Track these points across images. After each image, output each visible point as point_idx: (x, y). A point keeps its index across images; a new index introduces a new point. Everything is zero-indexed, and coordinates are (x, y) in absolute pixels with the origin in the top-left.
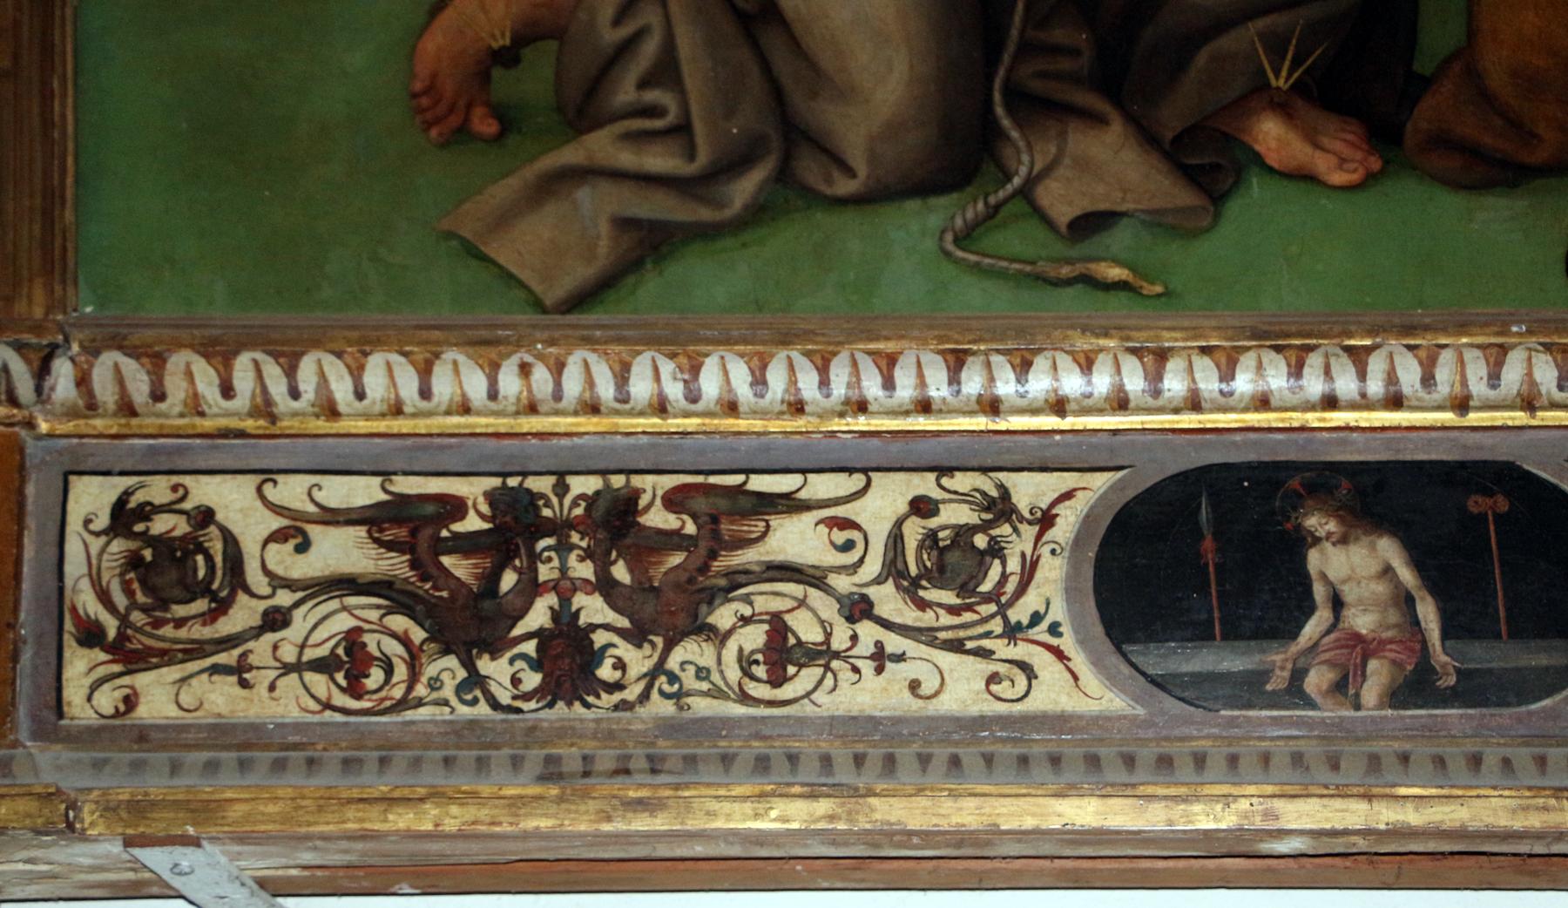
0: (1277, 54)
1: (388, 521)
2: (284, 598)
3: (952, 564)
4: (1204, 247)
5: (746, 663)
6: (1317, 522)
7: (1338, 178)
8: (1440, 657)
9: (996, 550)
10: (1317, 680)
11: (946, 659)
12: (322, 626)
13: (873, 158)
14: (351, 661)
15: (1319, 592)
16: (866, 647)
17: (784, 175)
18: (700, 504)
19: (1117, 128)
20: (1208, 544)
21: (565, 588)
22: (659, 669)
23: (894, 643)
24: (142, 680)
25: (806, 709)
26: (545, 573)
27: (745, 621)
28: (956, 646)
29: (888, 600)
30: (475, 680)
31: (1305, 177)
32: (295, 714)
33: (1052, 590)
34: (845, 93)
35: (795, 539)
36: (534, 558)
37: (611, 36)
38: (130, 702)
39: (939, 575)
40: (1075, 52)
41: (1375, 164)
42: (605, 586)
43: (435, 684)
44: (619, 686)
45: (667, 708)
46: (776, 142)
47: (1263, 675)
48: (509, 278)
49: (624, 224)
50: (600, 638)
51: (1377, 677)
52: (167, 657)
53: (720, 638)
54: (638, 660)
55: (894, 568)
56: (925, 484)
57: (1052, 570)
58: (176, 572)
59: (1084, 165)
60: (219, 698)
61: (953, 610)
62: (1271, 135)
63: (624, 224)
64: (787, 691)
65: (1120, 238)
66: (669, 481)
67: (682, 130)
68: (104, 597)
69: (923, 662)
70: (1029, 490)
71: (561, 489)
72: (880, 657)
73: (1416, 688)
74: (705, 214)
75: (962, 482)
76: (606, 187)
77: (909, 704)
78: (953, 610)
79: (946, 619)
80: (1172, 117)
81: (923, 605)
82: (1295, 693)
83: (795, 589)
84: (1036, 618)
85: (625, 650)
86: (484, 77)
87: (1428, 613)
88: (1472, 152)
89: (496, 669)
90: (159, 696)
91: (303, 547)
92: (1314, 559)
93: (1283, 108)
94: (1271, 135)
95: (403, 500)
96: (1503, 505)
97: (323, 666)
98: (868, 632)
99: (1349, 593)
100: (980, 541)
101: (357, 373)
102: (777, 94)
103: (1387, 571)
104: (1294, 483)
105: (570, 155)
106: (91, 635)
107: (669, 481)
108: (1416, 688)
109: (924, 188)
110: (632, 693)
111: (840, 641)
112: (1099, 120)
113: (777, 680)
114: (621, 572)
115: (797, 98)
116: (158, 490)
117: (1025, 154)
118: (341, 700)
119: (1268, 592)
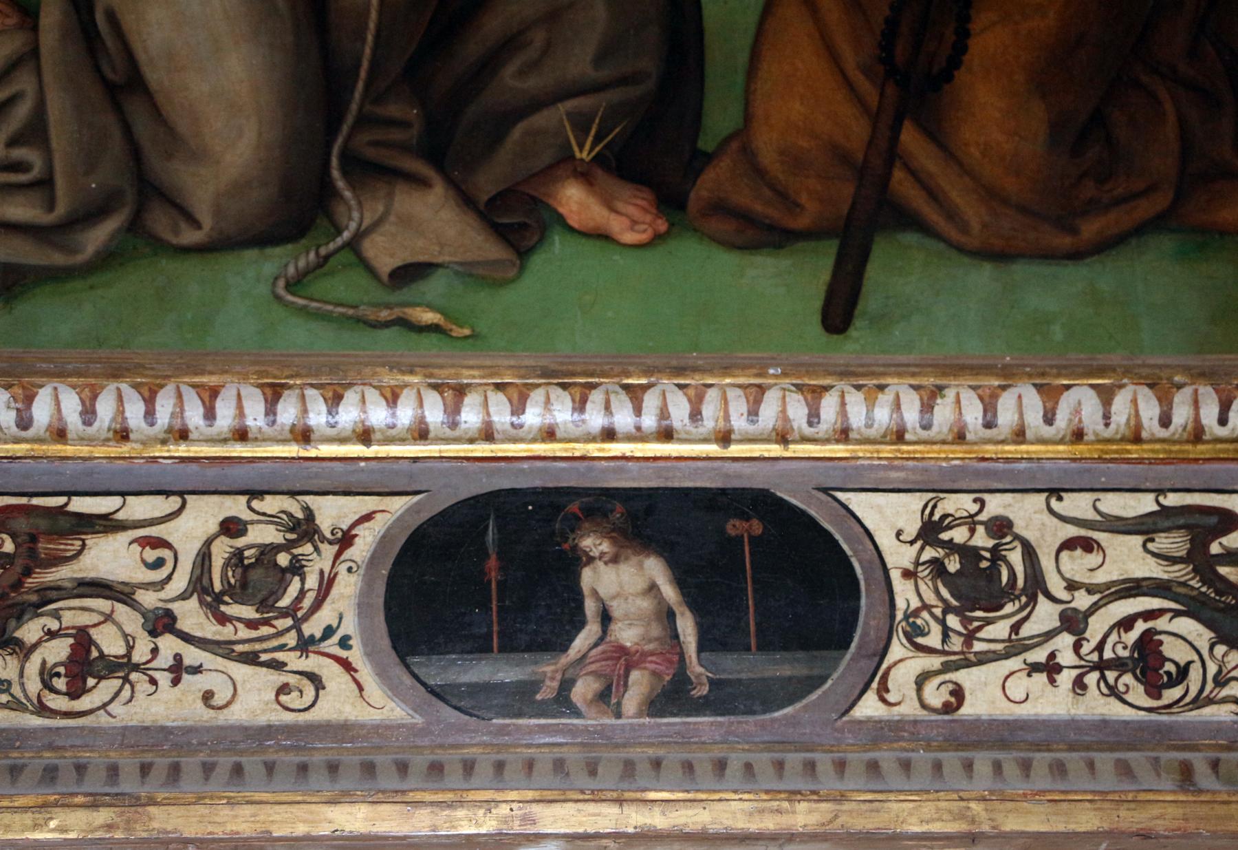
3: (254, 581)
4: (509, 295)
5: (47, 676)
6: (594, 543)
7: (629, 237)
8: (695, 668)
9: (297, 568)
11: (241, 671)
13: (218, 212)
15: (590, 607)
16: (165, 660)
17: (135, 226)
18: (22, 524)
23: (192, 655)
25: (102, 719)
27: (52, 635)
28: (251, 659)
29: (191, 616)
31: (602, 236)
33: (347, 605)
34: (199, 155)
35: (109, 557)
39: (240, 592)
40: (404, 124)
41: (662, 226)
46: (130, 196)
47: (533, 686)
51: (639, 685)
53: (25, 651)
55: (199, 586)
56: (236, 507)
57: (347, 587)
59: (406, 222)
61: (251, 624)
62: (573, 200)
64: (85, 703)
65: (435, 286)
67: (45, 184)
69: (218, 674)
70: (332, 512)
73: (672, 697)
74: (58, 259)
75: (271, 504)
78: (251, 624)
79: (244, 633)
80: (487, 183)
81: (223, 619)
82: (563, 702)
83: (103, 604)
84: (329, 632)
87: (687, 626)
88: (745, 218)
93: (585, 176)
94: (573, 200)
96: (757, 527)
98: (169, 645)
100: (283, 559)
102: (135, 153)
103: (653, 588)
104: (574, 507)
108: (672, 697)
109: (263, 239)
111: (141, 654)
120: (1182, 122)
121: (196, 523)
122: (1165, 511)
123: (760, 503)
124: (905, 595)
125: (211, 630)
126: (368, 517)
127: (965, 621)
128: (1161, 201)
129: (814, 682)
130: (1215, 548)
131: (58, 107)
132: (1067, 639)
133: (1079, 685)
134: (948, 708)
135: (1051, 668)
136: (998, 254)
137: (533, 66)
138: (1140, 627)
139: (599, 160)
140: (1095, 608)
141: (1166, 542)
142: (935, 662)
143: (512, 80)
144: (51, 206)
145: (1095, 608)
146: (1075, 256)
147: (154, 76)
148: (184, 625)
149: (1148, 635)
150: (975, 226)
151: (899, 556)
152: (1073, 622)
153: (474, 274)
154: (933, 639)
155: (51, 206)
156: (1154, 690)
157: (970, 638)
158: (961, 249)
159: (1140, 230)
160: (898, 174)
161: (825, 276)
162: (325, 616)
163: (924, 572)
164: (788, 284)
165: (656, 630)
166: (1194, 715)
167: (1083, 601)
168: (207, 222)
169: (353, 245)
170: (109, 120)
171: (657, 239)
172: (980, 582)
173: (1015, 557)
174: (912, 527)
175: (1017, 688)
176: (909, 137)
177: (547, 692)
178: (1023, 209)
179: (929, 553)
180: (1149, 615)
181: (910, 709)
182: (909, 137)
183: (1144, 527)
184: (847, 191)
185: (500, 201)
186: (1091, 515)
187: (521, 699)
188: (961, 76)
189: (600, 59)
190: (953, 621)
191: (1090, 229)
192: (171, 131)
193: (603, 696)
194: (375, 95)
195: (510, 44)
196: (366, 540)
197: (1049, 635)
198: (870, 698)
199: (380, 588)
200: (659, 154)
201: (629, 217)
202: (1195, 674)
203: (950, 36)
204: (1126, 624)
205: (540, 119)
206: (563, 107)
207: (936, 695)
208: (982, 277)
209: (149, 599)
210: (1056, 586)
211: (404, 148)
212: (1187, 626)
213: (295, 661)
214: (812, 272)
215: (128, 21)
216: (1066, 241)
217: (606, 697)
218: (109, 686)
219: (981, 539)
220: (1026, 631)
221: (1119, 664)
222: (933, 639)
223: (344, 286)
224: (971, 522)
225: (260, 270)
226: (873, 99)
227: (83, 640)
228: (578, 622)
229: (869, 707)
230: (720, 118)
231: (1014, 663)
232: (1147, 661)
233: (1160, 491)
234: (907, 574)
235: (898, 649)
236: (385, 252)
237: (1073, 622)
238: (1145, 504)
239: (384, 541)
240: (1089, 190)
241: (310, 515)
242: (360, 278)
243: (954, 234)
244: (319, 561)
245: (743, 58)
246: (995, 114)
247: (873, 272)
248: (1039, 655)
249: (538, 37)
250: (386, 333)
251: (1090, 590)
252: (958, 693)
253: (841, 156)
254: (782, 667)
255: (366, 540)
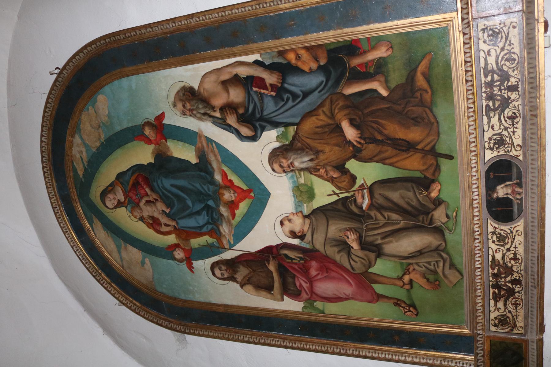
0: (422, 194)
1: (496, 298)
2: (507, 311)
3: (502, 239)
4: (450, 203)
5: (516, 263)
6: (495, 196)
7: (439, 187)
8: (515, 182)
9: (500, 234)
10: (518, 197)
11: (515, 240)
12: (510, 307)
13: (440, 241)
14: (516, 305)
15: (505, 196)
16: (514, 249)
17: (442, 251)
18: (493, 266)
19: (434, 213)
20: (498, 209)
21: (505, 282)
22: (517, 272)
23: (513, 246)
24: (518, 325)
25: (523, 256)
26: (503, 284)
27: (510, 262)
28: (514, 239)
29: (507, 246)
30: (518, 292)
31: (440, 191)
32: (523, 311)
33: (505, 228)
34: (431, 243)
35: (498, 256)
36: (501, 285)
37: (424, 268)
38: (521, 327)
39: (503, 240)
40: (423, 218)
41: (437, 182)
42: (505, 277)
43: (519, 296)
44: (519, 277)
45: (522, 272)
46: (438, 252)
47: (518, 204)
48: (458, 281)
49: (450, 269)
50: (513, 278)
51: (518, 189)
52: (515, 323)
53: (513, 266)
54: (516, 274)
55: (503, 246)
56: (490, 241)
57: (503, 227)
58: (502, 321)
59: (439, 217)
60: (520, 318)
61: (509, 239)
62: (434, 195)
63: (450, 269)
64: (520, 258)
65: (450, 213)
66: (490, 270)
67: (437, 262)
68: (506, 328)
69: (516, 242)
70: (491, 229)
71: (491, 281)
72: (515, 248)
73: (520, 185)
74: (448, 260)
75: (490, 237)
76: (445, 270)
77: (522, 245)
78: (509, 239)
79: (510, 240)
80: (432, 206)
81: (508, 243)
82: (521, 200)
83: (505, 257)
84: (510, 230)
85: (514, 276)
86: (431, 282)
87: (508, 183)
88: (435, 171)
89: (517, 290)
90: (520, 324)
91: (500, 309)
92: (500, 197)
93: (430, 193)
94: (434, 195)
95: (493, 298)
96: (491, 173)
97: (516, 308)
98: (511, 249)
99: (506, 193)
100: (498, 235)
101: (478, 303)
102: (431, 251)
103: (502, 188)
104: (489, 198)
105: (441, 274)
106: (512, 330)
107: (490, 270)
108: (520, 185)
109: (443, 235)
110: (520, 275)
111: (513, 252)
112: (433, 215)
113: (519, 259)
114: (503, 276)
115: (432, 249)
116: (492, 322)
117: (438, 223)
118: (521, 306)
119: (506, 202)
122: (486, 115)
123: (487, 173)
124: (502, 153)
127: (506, 144)
128: (427, 110)
130: (492, 108)
132: (509, 130)
133: (516, 128)
134: (521, 147)
135: (514, 132)
136: (438, 134)
137: (412, 200)
138: (506, 119)
140: (503, 125)
141: (492, 114)
142: (513, 149)
143: (414, 203)
145: (503, 125)
146: (438, 123)
147: (418, 249)
148: (509, 247)
149: (507, 118)
150: (434, 138)
151: (496, 153)
152: (506, 129)
154: (509, 149)
156: (517, 117)
157: (509, 144)
158: (438, 140)
159: (432, 112)
160: (425, 149)
161: (444, 159)
162: (507, 230)
163: (498, 150)
164: (445, 164)
165: (509, 187)
166: (521, 111)
167: (502, 127)
168: (441, 242)
169: (444, 224)
170: (426, 254)
172: (500, 142)
173: (495, 137)
174: (491, 152)
175: (517, 136)
176: (419, 147)
177: (519, 202)
179: (495, 149)
180: (504, 117)
181: (521, 152)
182: (419, 147)
183: (489, 118)
184: (429, 156)
186: (487, 126)
188: (407, 140)
189: (410, 191)
190: (506, 146)
191: (433, 120)
193: (519, 194)
194: (419, 221)
195: (408, 203)
196: (495, 225)
198: (519, 158)
200: (425, 183)
202: (514, 111)
203: (401, 141)
204: (506, 121)
205: (421, 199)
206: (418, 196)
207: (519, 148)
208: (442, 137)
209: (505, 252)
211: (427, 217)
212: (506, 112)
214: (444, 162)
215: (410, 252)
216: (435, 124)
218: (518, 255)
219: (492, 142)
220: (507, 135)
221: (513, 122)
223: (450, 225)
224: (489, 143)
226: (413, 153)
230: (418, 174)
231: (513, 137)
232: (512, 118)
233: (483, 115)
234: (499, 152)
235: (511, 154)
236: (445, 220)
237: (506, 129)
238: (485, 118)
242: (449, 223)
243: (435, 141)
245: (407, 171)
246: (414, 134)
247: (443, 152)
248: (512, 134)
249: (406, 200)
251: (500, 126)
252: (518, 145)
253: (423, 157)
254: (514, 170)
255: (495, 225)
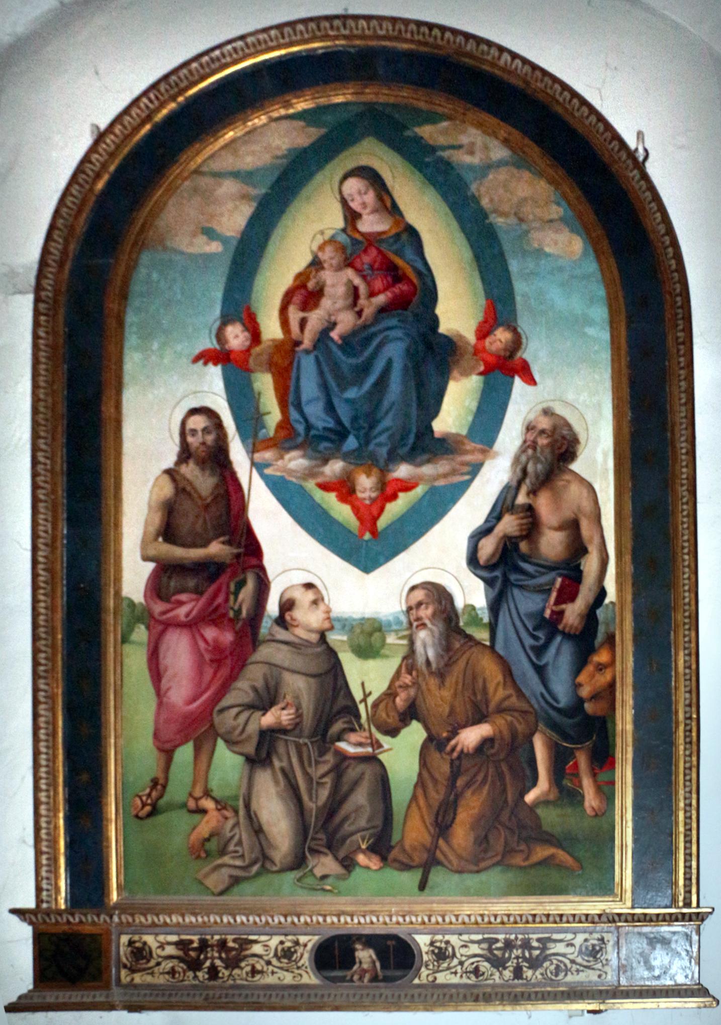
4: (347, 882)
5: (247, 973)
6: (358, 946)
9: (296, 952)
11: (285, 973)
13: (281, 863)
15: (357, 960)
16: (270, 970)
17: (263, 866)
23: (275, 970)
27: (247, 965)
28: (287, 970)
29: (275, 961)
31: (368, 868)
33: (306, 959)
35: (257, 949)
39: (285, 956)
47: (345, 977)
51: (367, 977)
53: (242, 969)
55: (276, 955)
56: (282, 938)
57: (306, 956)
59: (323, 864)
62: (361, 858)
64: (255, 979)
65: (330, 880)
67: (242, 856)
70: (303, 939)
73: (375, 979)
75: (290, 937)
80: (342, 854)
83: (256, 959)
87: (378, 965)
88: (402, 863)
93: (363, 852)
94: (361, 858)
96: (394, 942)
98: (271, 968)
102: (262, 850)
103: (371, 957)
104: (354, 938)
108: (375, 979)
109: (292, 868)
111: (265, 969)
120: (506, 837)
121: (274, 941)
122: (484, 939)
124: (425, 958)
125: (278, 964)
126: (310, 941)
128: (499, 858)
129: (405, 976)
130: (494, 947)
131: (245, 837)
133: (461, 976)
135: (456, 973)
136: (460, 872)
137: (353, 823)
139: (367, 848)
141: (485, 946)
142: (431, 972)
144: (244, 861)
146: (478, 872)
147: (265, 828)
150: (455, 864)
151: (424, 949)
152: (461, 963)
153: (339, 877)
154: (431, 967)
155: (244, 861)
156: (477, 977)
157: (439, 967)
158: (452, 871)
159: (494, 865)
164: (411, 879)
167: (464, 959)
169: (311, 871)
170: (255, 839)
171: (381, 868)
172: (441, 955)
173: (450, 949)
174: (428, 942)
175: (448, 977)
177: (348, 978)
178: (467, 861)
180: (478, 962)
181: (425, 981)
183: (479, 942)
185: (346, 858)
187: (343, 979)
188: (454, 825)
190: (436, 963)
191: (483, 865)
192: (270, 842)
195: (346, 818)
197: (455, 966)
199: (313, 956)
201: (374, 862)
203: (452, 815)
204: (473, 963)
206: (359, 834)
207: (431, 979)
208: (456, 877)
209: (266, 958)
210: (458, 955)
211: (322, 846)
213: (296, 971)
214: (417, 875)
216: (476, 868)
217: (361, 979)
219: (443, 945)
221: (470, 972)
222: (431, 967)
223: (309, 880)
224: (441, 941)
225: (292, 876)
227: (253, 967)
228: (354, 963)
229: (416, 981)
230: (396, 837)
231: (448, 972)
232: (476, 971)
233: (483, 934)
235: (423, 969)
236: (318, 872)
237: (461, 963)
238: (480, 937)
239: (314, 946)
240: (482, 855)
241: (298, 940)
243: (450, 867)
244: (300, 950)
246: (462, 835)
248: (453, 970)
249: (353, 815)
250: (318, 892)
252: (435, 978)
253: (424, 846)
254: (398, 973)
